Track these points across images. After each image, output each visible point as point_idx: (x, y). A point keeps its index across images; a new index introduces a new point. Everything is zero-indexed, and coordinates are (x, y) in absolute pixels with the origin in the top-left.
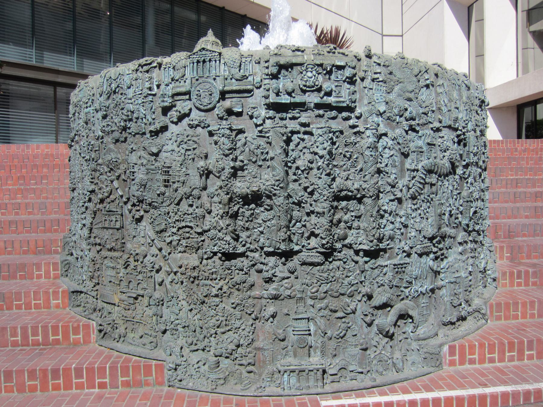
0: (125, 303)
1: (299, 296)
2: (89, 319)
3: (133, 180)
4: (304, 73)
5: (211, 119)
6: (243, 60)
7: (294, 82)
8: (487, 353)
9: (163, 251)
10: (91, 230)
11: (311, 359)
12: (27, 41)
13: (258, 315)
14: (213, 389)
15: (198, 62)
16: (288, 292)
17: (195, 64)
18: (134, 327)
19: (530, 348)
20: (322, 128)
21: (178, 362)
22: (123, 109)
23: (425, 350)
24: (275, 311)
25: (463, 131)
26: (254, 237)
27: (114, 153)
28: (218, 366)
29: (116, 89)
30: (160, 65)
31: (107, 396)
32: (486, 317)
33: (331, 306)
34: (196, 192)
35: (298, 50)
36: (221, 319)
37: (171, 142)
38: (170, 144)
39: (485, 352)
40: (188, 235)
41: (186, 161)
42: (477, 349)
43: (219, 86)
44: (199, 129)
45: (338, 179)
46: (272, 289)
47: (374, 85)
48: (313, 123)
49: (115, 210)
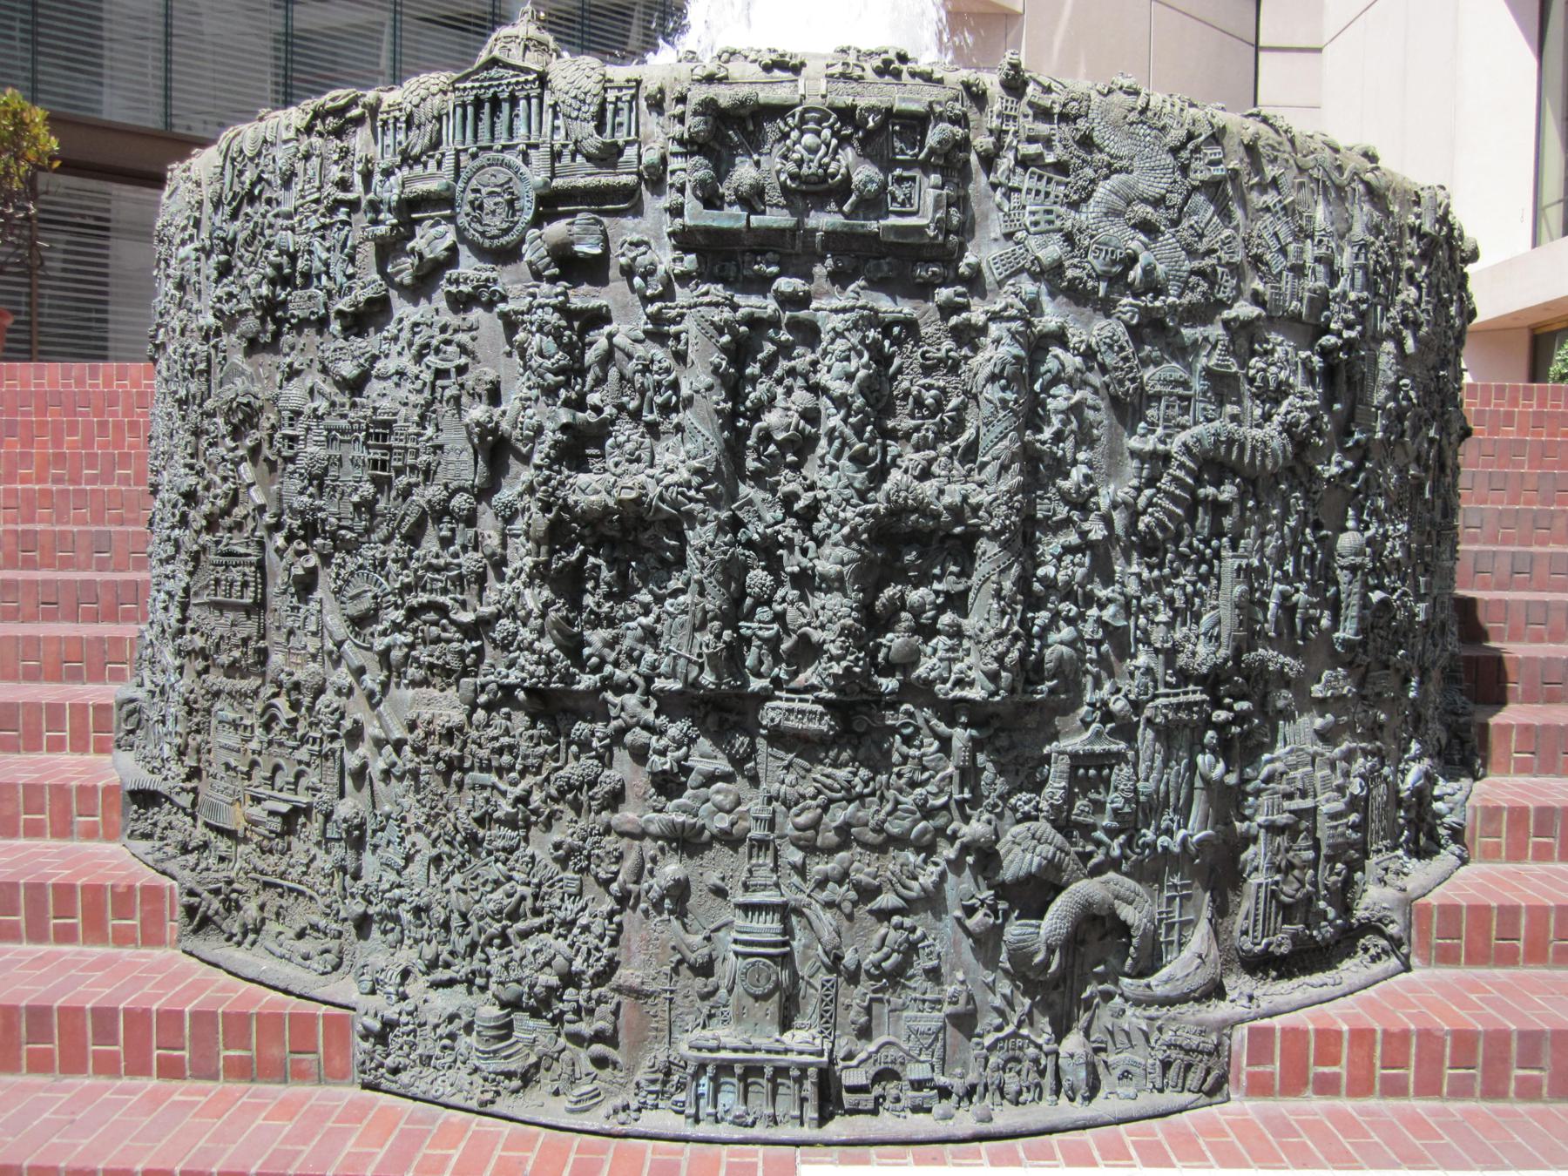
0: (261, 830)
1: (757, 833)
2: (164, 873)
3: (292, 460)
4: (795, 134)
5: (512, 282)
6: (611, 96)
7: (764, 166)
8: (1378, 1063)
9: (366, 677)
10: (184, 607)
11: (787, 1037)
12: (149, 62)
13: (630, 886)
14: (483, 1104)
15: (478, 103)
16: (722, 822)
17: (470, 109)
18: (283, 902)
19: (1529, 1060)
20: (844, 310)
21: (391, 1013)
22: (268, 246)
23: (1168, 1036)
24: (680, 875)
25: (1346, 334)
26: (626, 644)
27: (248, 378)
28: (508, 1036)
29: (253, 185)
30: (374, 109)
31: (176, 1097)
32: (1404, 950)
33: (858, 871)
34: (460, 502)
35: (780, 64)
36: (521, 889)
37: (397, 348)
38: (394, 353)
39: (1371, 1057)
40: (435, 630)
41: (437, 406)
42: (1345, 1044)
43: (536, 173)
44: (477, 314)
45: (895, 475)
46: (674, 813)
47: (1024, 181)
48: (820, 296)
49: (242, 550)
